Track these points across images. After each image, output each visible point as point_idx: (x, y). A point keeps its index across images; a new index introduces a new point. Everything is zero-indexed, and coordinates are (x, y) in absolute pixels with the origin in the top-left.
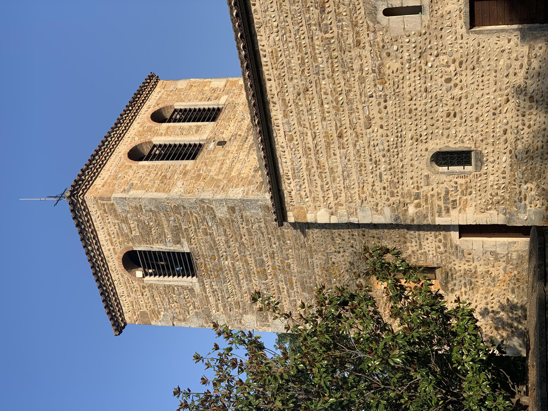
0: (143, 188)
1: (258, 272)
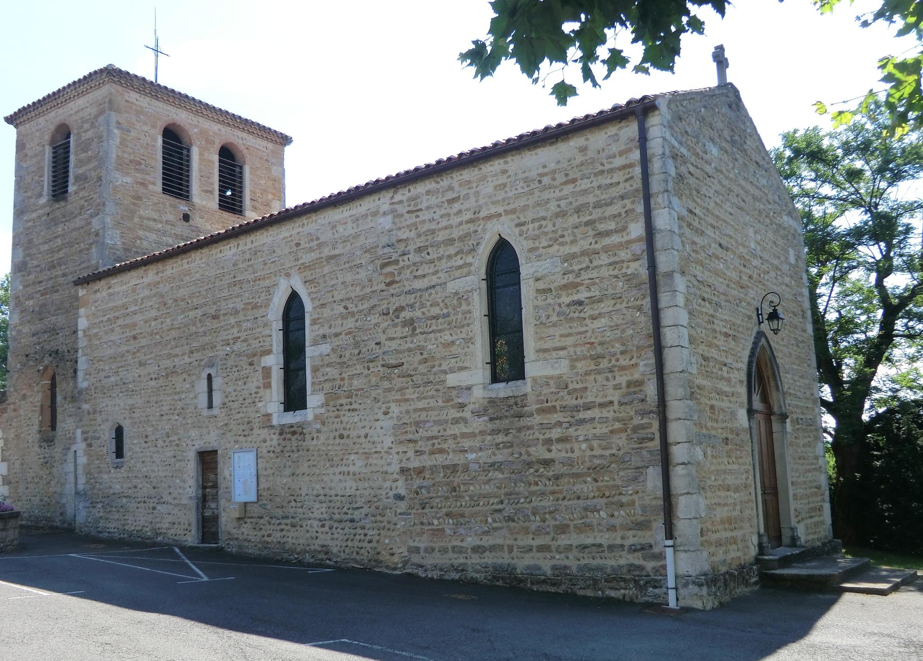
0: (123, 142)
1: (53, 261)
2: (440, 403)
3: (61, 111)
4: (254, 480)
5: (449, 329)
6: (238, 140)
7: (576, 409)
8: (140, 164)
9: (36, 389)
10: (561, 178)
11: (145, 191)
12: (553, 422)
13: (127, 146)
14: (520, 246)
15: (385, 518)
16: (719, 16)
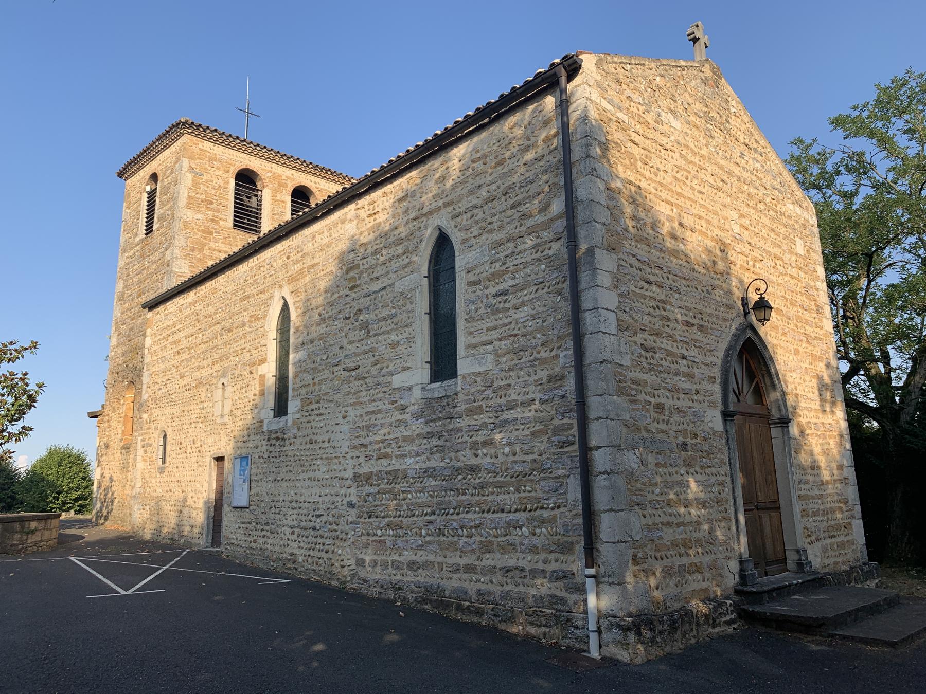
0: (195, 184)
14: (456, 237)
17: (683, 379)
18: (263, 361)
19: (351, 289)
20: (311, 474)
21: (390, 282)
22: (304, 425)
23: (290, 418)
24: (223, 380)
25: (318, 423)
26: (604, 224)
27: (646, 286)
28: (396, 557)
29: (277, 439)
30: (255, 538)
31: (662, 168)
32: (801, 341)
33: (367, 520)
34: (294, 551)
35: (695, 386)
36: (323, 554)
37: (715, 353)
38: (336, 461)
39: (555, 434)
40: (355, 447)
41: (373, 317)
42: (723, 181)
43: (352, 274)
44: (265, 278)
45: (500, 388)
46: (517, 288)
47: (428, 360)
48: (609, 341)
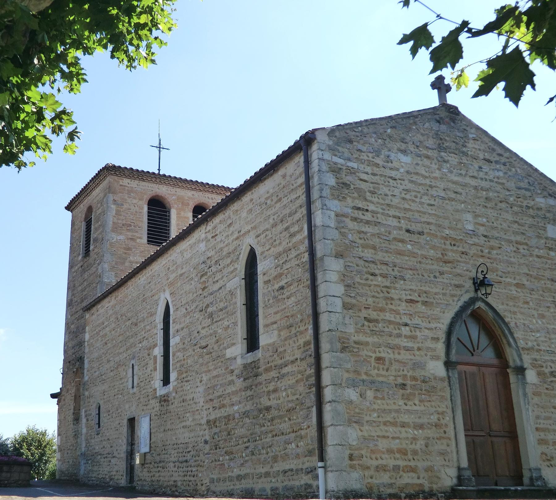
0: (118, 213)
2: (223, 371)
3: (89, 198)
4: (148, 436)
5: (228, 317)
6: (208, 200)
7: (281, 367)
8: (130, 225)
9: (73, 384)
10: (275, 199)
11: (134, 244)
12: (271, 378)
13: (120, 215)
14: (258, 251)
15: (200, 458)
16: (411, 56)
17: (405, 340)
18: (155, 346)
19: (203, 289)
20: (184, 424)
21: (224, 284)
22: (179, 389)
23: (171, 386)
24: (133, 362)
25: (187, 386)
26: (333, 240)
27: (371, 277)
28: (230, 474)
29: (165, 401)
30: (154, 473)
31: (390, 193)
32: (548, 307)
33: (215, 451)
34: (176, 479)
35: (417, 345)
36: (192, 479)
37: (442, 321)
38: (197, 413)
39: (307, 380)
40: (207, 402)
41: (215, 308)
42: (456, 192)
43: (204, 279)
44: (156, 285)
45: (281, 352)
46: (289, 284)
47: (246, 337)
48: (334, 318)
